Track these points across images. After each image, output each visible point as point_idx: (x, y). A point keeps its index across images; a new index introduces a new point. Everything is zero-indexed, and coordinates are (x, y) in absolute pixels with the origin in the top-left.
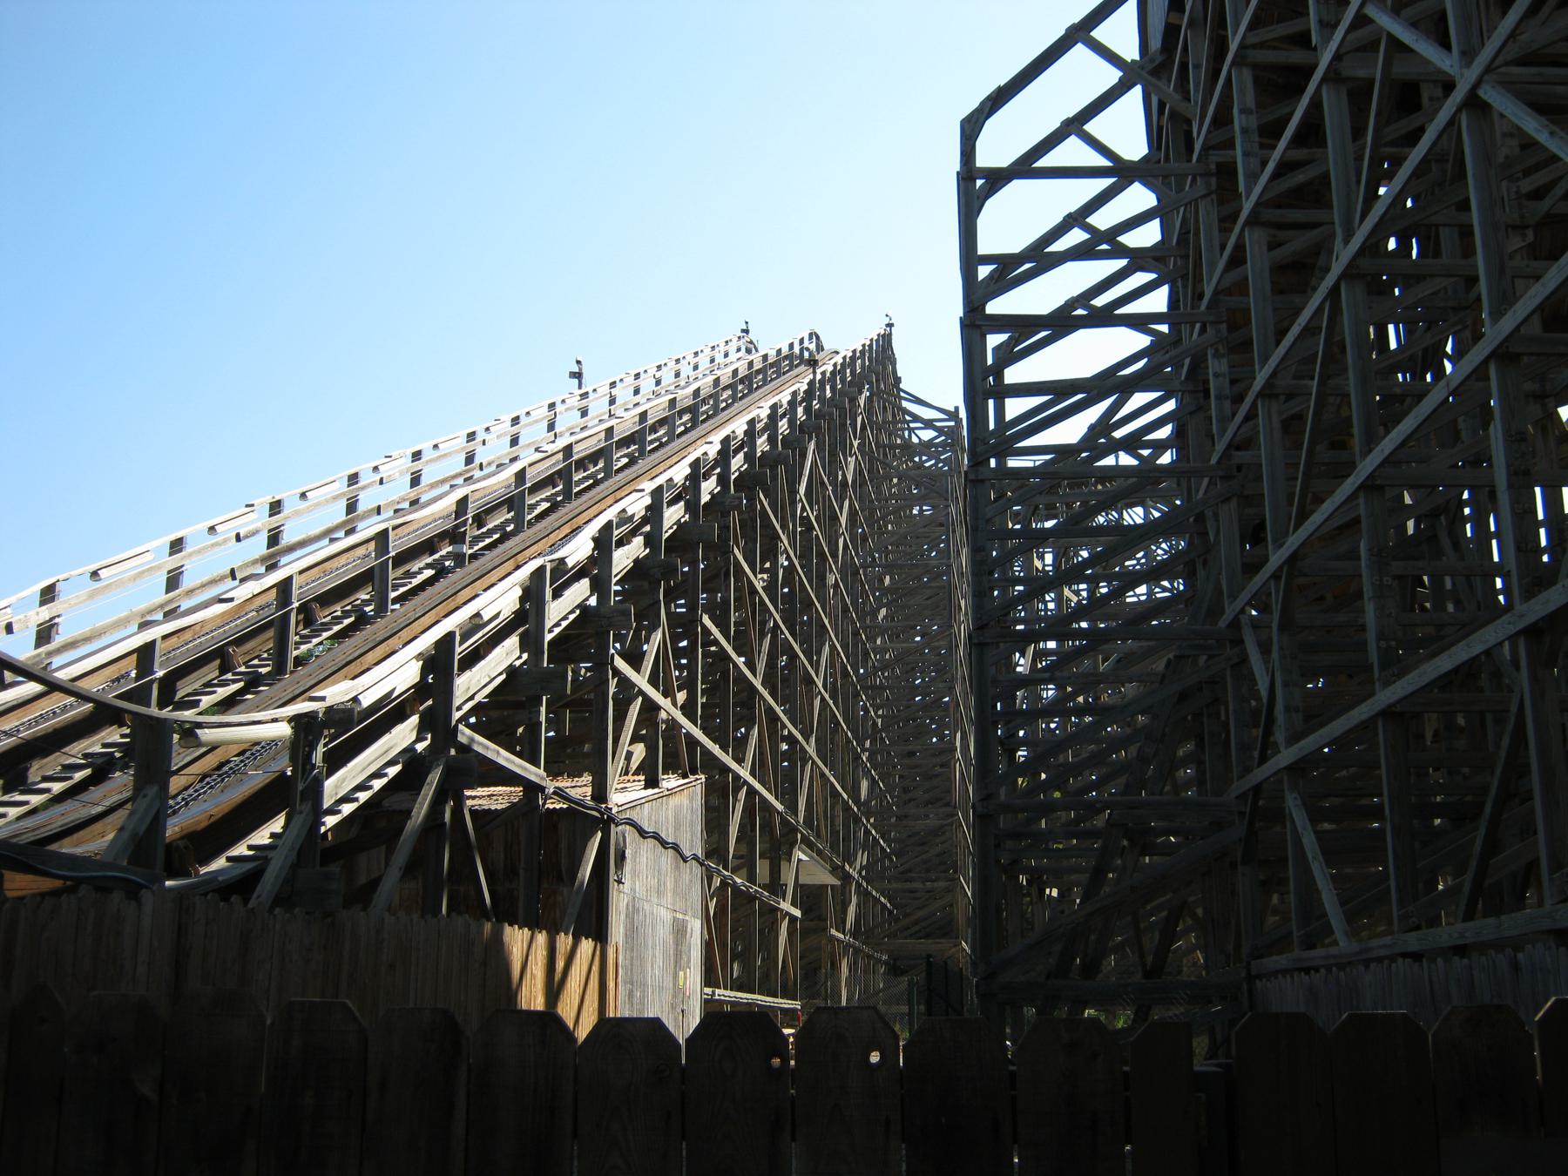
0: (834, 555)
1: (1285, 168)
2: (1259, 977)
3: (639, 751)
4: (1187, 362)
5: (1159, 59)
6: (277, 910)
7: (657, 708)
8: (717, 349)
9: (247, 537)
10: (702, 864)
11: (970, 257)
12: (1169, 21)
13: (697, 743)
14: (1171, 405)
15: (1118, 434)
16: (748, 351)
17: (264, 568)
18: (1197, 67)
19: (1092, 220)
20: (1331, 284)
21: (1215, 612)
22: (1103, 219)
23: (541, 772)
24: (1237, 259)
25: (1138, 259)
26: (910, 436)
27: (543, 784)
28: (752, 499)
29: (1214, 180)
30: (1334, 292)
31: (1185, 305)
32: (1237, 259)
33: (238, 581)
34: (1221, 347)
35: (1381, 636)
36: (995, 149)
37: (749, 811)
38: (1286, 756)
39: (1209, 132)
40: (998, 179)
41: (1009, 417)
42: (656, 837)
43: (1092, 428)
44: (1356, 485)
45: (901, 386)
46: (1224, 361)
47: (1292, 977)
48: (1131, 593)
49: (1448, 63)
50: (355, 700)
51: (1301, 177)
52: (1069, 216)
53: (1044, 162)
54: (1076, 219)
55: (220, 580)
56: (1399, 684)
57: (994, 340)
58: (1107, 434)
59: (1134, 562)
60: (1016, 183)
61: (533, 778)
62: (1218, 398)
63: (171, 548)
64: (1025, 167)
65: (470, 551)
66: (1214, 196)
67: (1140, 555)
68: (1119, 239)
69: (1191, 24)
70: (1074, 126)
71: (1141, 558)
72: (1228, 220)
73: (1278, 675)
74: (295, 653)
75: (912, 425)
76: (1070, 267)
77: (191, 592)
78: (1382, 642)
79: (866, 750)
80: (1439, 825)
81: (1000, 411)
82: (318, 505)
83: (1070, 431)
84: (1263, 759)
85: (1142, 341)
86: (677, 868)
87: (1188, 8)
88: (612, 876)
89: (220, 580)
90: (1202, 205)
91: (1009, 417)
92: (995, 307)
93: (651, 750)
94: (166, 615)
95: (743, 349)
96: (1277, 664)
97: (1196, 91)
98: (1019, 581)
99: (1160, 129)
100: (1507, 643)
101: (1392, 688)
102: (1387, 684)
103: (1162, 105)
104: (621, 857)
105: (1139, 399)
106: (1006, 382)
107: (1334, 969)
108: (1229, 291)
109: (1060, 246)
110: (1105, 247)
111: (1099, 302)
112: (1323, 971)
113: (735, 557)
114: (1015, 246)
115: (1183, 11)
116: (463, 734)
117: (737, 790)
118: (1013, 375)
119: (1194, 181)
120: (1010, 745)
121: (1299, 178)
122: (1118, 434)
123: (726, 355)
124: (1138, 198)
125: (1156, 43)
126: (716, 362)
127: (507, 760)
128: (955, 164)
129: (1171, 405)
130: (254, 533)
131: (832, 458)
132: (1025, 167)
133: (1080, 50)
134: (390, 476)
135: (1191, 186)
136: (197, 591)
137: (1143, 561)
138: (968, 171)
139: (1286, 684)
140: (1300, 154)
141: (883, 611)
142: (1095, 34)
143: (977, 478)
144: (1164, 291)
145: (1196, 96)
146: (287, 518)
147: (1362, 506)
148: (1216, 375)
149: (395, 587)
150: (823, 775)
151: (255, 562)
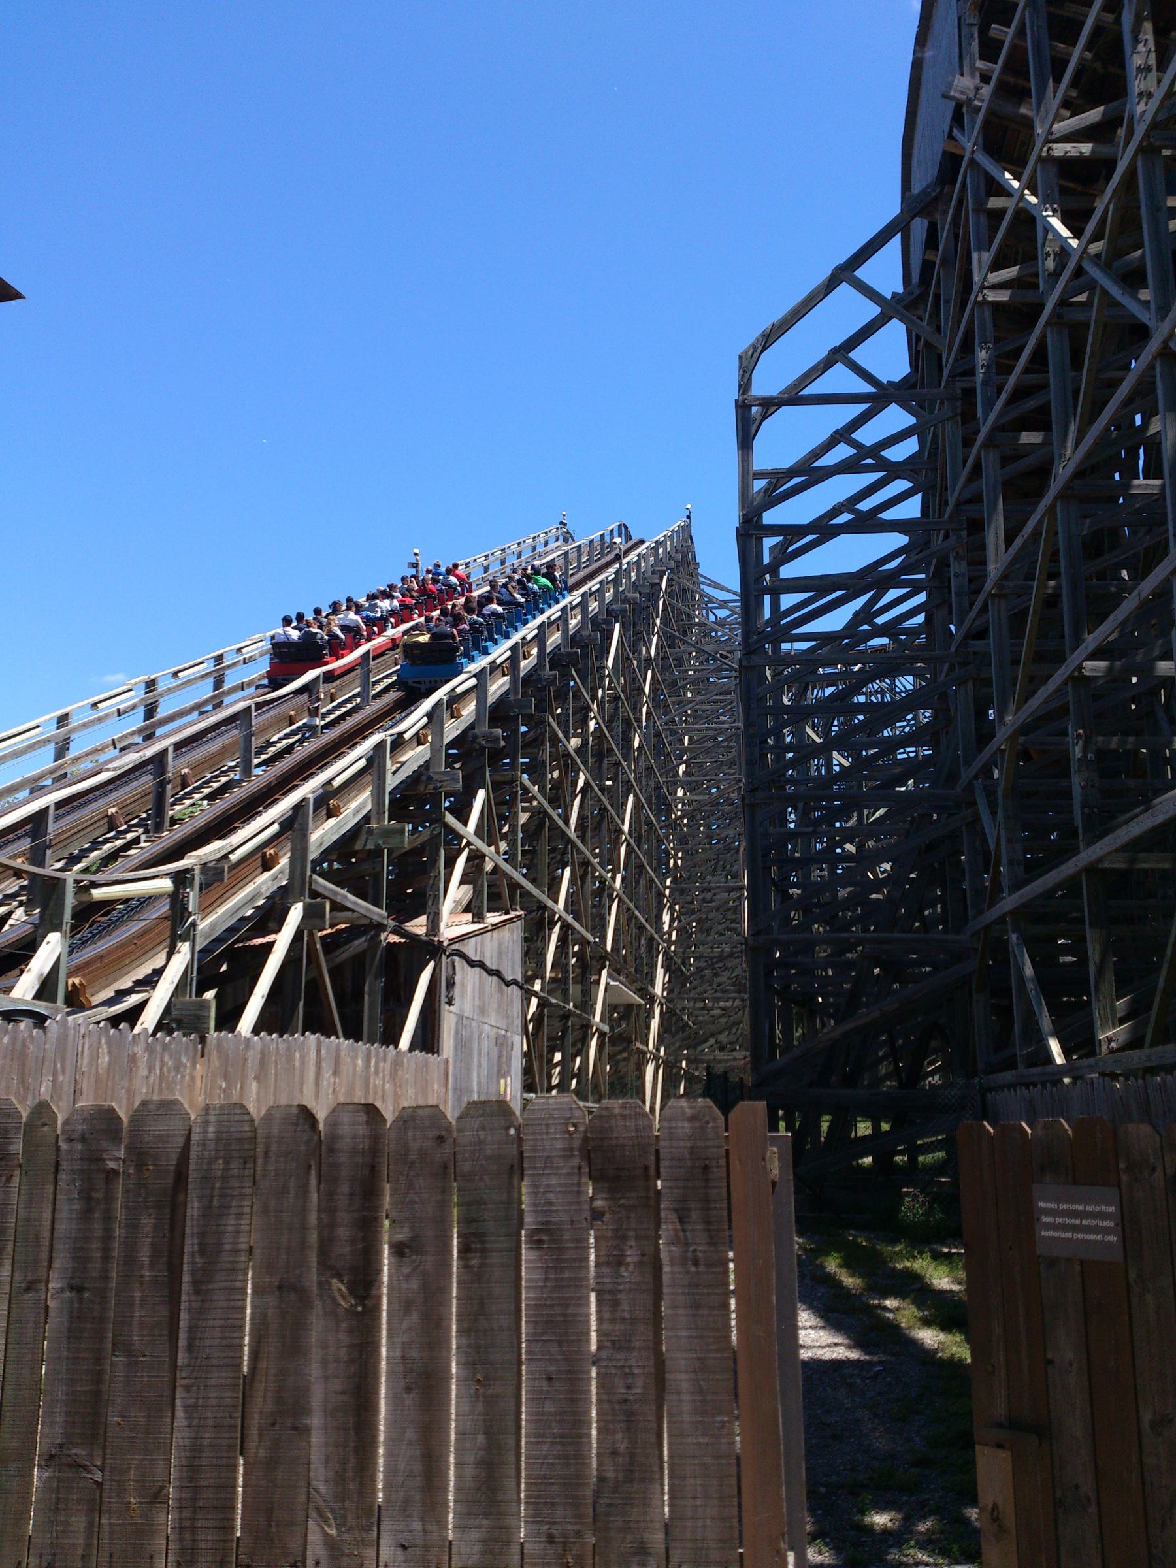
0: (639, 721)
1: (1018, 395)
2: (990, 1090)
3: (466, 892)
4: (934, 561)
5: (917, 292)
6: (159, 1035)
7: (482, 856)
8: (538, 540)
9: (125, 712)
10: (521, 988)
11: (747, 474)
12: (926, 257)
13: (518, 886)
14: (921, 598)
15: (880, 620)
16: (566, 540)
17: (141, 738)
18: (947, 301)
19: (858, 435)
20: (1049, 503)
21: (953, 777)
22: (868, 435)
23: (384, 913)
24: (977, 469)
25: (893, 471)
26: (707, 614)
27: (385, 922)
28: (566, 676)
29: (959, 404)
30: (1051, 509)
31: (934, 515)
32: (977, 469)
33: (118, 750)
34: (961, 551)
35: (1084, 805)
36: (767, 383)
37: (563, 940)
38: (1009, 902)
39: (956, 360)
40: (770, 405)
41: (783, 607)
42: (481, 965)
43: (856, 615)
44: (1065, 676)
45: (700, 571)
46: (964, 563)
47: (1015, 1091)
48: (902, 750)
49: (1147, 316)
50: (226, 856)
51: (1032, 403)
52: (836, 432)
53: (811, 390)
54: (842, 435)
55: (101, 750)
56: (1099, 845)
57: (769, 542)
58: (870, 622)
59: (905, 723)
60: (785, 409)
61: (376, 918)
62: (958, 595)
63: (58, 723)
64: (794, 397)
65: (322, 723)
66: (959, 418)
67: (910, 717)
68: (883, 453)
69: (944, 262)
70: (841, 354)
71: (910, 720)
72: (968, 442)
73: (1003, 833)
74: (171, 813)
75: (709, 605)
76: (804, 519)
77: (76, 760)
78: (1087, 809)
79: (668, 887)
80: (827, 1114)
81: (775, 604)
82: (188, 682)
83: (835, 621)
84: (992, 903)
85: (899, 540)
86: (501, 991)
87: (941, 247)
88: (443, 999)
89: (101, 750)
90: (949, 425)
91: (783, 607)
92: (771, 517)
93: (477, 893)
94: (56, 780)
95: (561, 538)
96: (1002, 825)
97: (946, 324)
98: (789, 748)
99: (917, 352)
100: (1084, 875)
101: (1092, 848)
102: (1089, 844)
103: (918, 338)
104: (451, 984)
105: (893, 594)
106: (782, 576)
107: (1048, 1084)
108: (970, 501)
109: (828, 460)
110: (869, 461)
111: (865, 506)
112: (1039, 1086)
113: (550, 725)
114: (786, 463)
115: (938, 250)
116: (316, 883)
117: (552, 924)
118: (788, 571)
119: (942, 403)
120: (782, 886)
121: (1032, 403)
122: (880, 620)
123: (546, 544)
124: (896, 418)
125: (915, 277)
126: (537, 551)
127: (355, 903)
128: (733, 394)
129: (921, 598)
130: (134, 707)
131: (635, 639)
132: (794, 397)
133: (844, 289)
134: (251, 657)
135: (940, 409)
136: (83, 759)
137: (913, 722)
138: (742, 408)
139: (1009, 841)
140: (1033, 378)
141: (682, 768)
142: (858, 273)
143: (749, 673)
144: (917, 499)
145: (947, 328)
146: (161, 695)
147: (1070, 693)
148: (957, 575)
149: (259, 753)
150: (629, 909)
151: (133, 733)
